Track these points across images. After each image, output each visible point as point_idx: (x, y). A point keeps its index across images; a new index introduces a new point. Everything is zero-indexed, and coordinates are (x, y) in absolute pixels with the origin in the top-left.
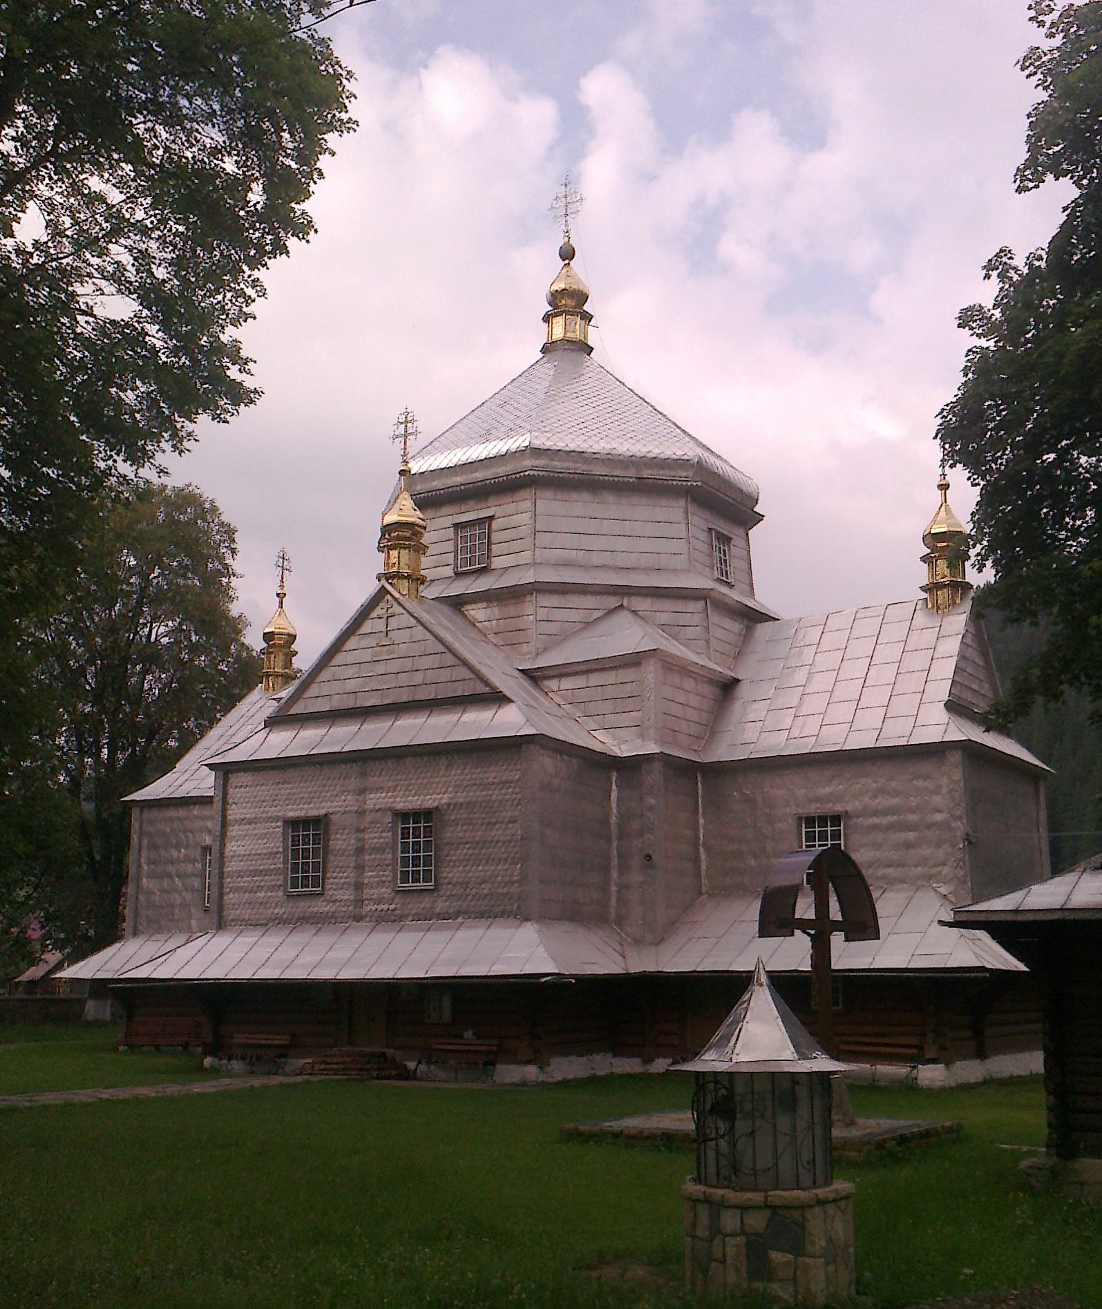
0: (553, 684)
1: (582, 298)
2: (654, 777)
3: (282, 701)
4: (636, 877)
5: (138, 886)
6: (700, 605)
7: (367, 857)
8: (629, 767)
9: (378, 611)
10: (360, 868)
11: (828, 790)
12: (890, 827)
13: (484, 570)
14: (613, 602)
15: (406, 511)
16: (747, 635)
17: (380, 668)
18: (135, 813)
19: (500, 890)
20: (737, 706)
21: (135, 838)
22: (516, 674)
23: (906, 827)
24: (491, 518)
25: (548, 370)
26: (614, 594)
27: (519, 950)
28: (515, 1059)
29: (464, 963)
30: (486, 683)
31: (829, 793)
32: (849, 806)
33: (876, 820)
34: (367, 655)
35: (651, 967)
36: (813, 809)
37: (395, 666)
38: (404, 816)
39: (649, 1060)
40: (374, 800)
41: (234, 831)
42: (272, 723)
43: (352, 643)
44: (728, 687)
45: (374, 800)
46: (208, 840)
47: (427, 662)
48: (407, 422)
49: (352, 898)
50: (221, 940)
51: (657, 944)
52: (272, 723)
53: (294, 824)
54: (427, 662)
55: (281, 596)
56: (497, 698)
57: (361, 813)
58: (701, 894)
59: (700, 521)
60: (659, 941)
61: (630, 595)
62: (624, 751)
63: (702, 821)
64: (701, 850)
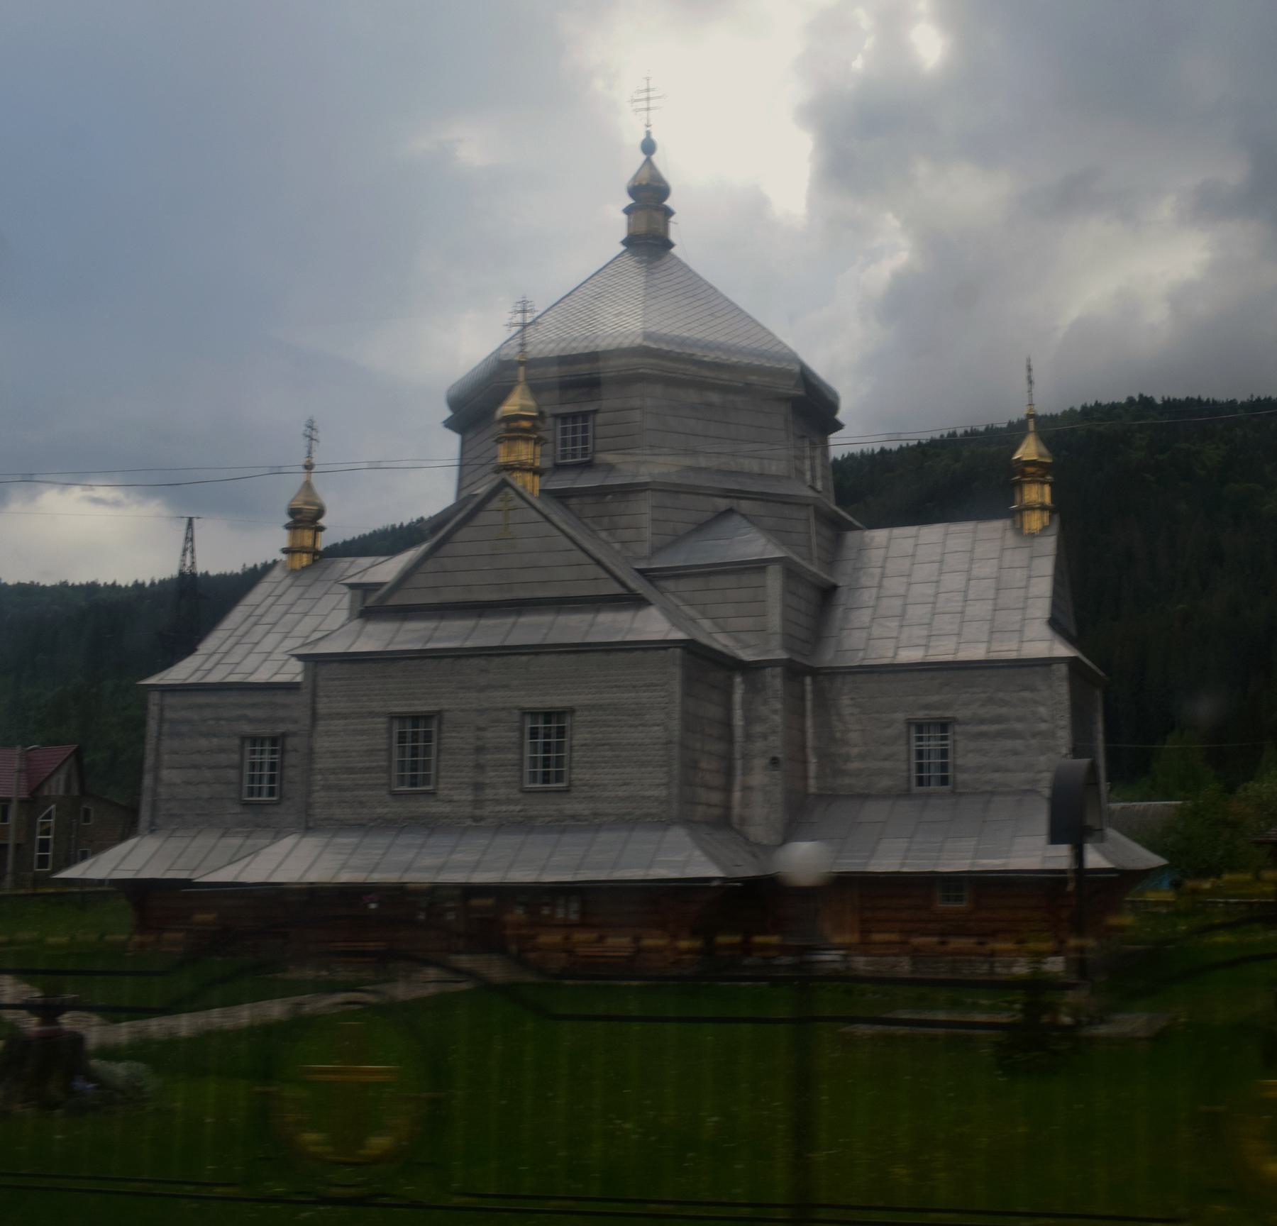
0: (670, 585)
5: (157, 779)
13: (588, 466)
14: (723, 503)
18: (154, 697)
21: (152, 726)
24: (595, 412)
30: (623, 584)
32: (961, 713)
33: (984, 728)
49: (470, 798)
62: (747, 655)
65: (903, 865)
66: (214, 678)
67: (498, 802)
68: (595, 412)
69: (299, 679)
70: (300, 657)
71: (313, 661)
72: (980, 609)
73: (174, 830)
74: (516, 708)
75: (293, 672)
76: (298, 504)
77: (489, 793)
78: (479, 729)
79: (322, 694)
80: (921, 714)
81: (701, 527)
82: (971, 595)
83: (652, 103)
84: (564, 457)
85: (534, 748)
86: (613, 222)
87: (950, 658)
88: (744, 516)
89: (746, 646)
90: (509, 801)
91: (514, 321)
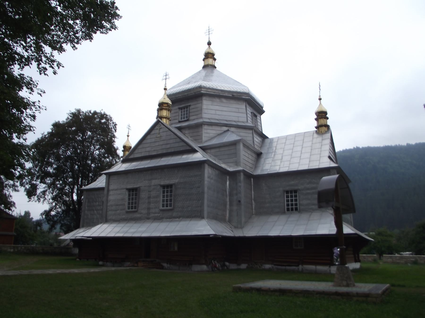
4: (235, 208)
6: (251, 132)
7: (151, 200)
8: (233, 175)
9: (157, 127)
10: (149, 203)
13: (188, 120)
14: (225, 128)
17: (157, 144)
24: (190, 106)
25: (204, 73)
26: (226, 126)
27: (203, 228)
28: (199, 263)
30: (190, 146)
31: (292, 184)
33: (308, 191)
34: (153, 140)
36: (287, 188)
37: (161, 143)
38: (164, 187)
39: (239, 264)
40: (154, 182)
41: (111, 193)
43: (149, 137)
44: (259, 155)
47: (171, 141)
50: (105, 226)
53: (130, 190)
54: (171, 141)
55: (128, 136)
56: (194, 151)
57: (150, 186)
58: (253, 214)
59: (250, 110)
60: (242, 228)
61: (231, 127)
63: (253, 192)
65: (280, 233)
68: (190, 106)
81: (219, 135)
82: (303, 152)
88: (232, 132)
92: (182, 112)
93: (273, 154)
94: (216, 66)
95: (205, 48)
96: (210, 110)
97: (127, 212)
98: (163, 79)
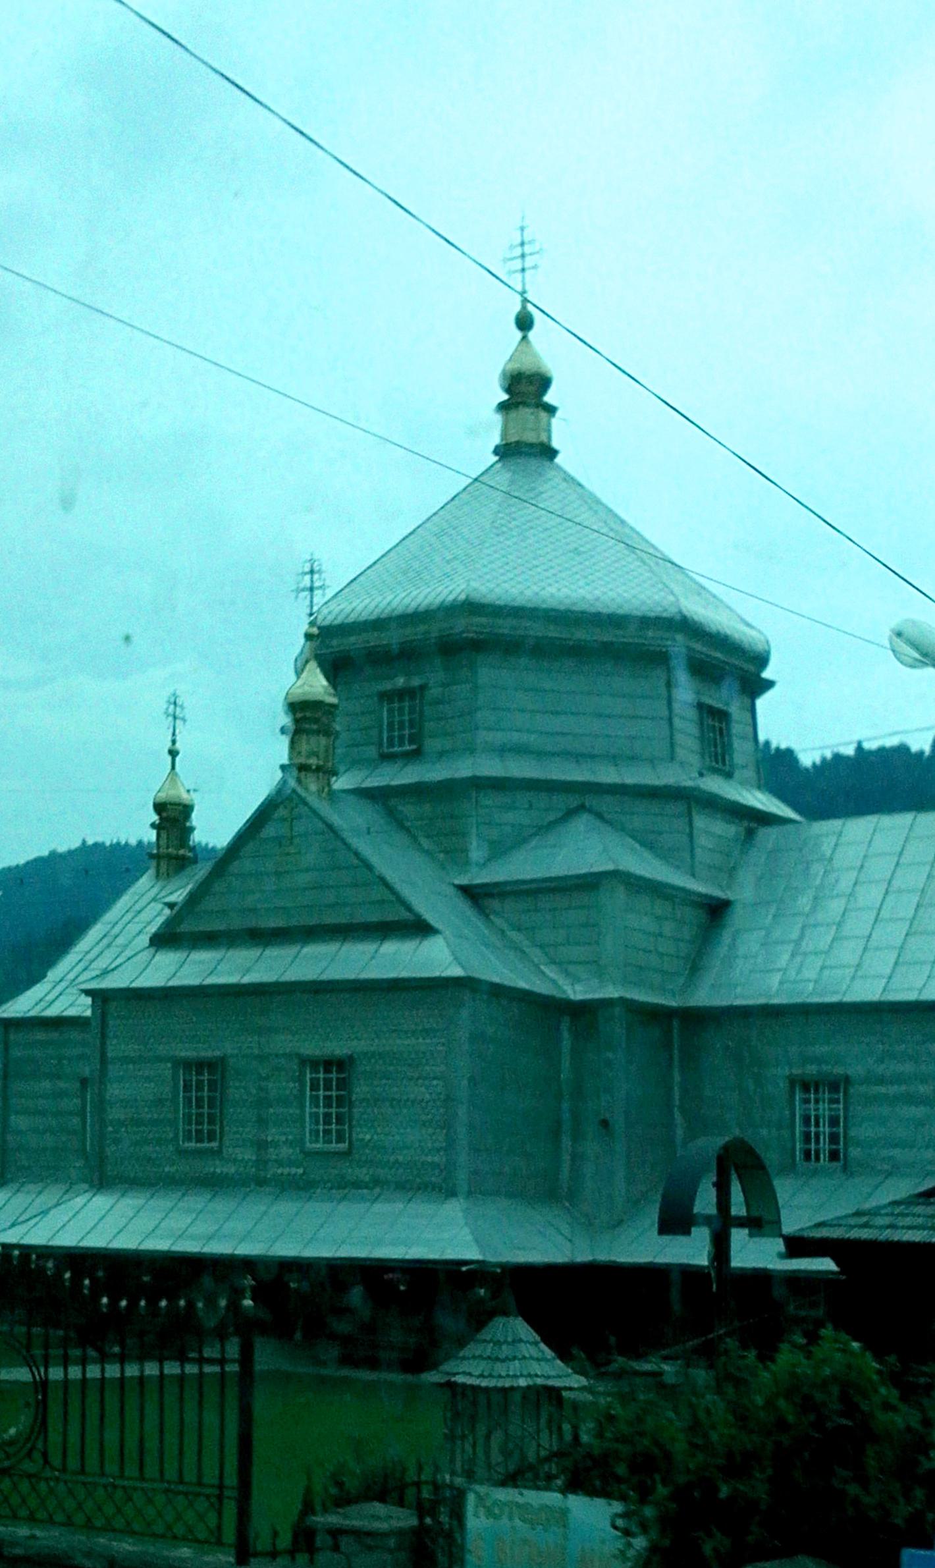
0: (495, 904)
1: (543, 382)
2: (616, 1028)
3: (176, 908)
4: (591, 1147)
11: (826, 1049)
12: (894, 1100)
13: (416, 755)
14: (573, 801)
15: (317, 684)
16: (750, 833)
19: (429, 1159)
20: (726, 936)
22: (451, 891)
23: (911, 1099)
25: (502, 478)
29: (380, 1242)
30: (409, 908)
32: (856, 1070)
35: (602, 1256)
40: (282, 1043)
42: (164, 940)
44: (716, 911)
45: (282, 1043)
46: (87, 1072)
48: (311, 589)
49: (254, 1158)
51: (614, 1227)
52: (164, 940)
55: (173, 753)
56: (420, 928)
62: (577, 993)
63: (677, 1077)
64: (677, 1114)
66: (52, 1012)
67: (280, 1163)
69: (88, 1013)
70: (88, 992)
71: (100, 997)
72: (894, 933)
73: (23, 1184)
74: (288, 1056)
75: (83, 1007)
76: (163, 797)
77: (272, 1153)
78: (261, 1078)
79: (111, 1034)
80: (812, 1069)
82: (885, 914)
83: (529, 261)
84: (401, 744)
85: (315, 1100)
86: (475, 426)
87: (912, 996)
89: (576, 979)
90: (291, 1163)
91: (302, 586)
92: (390, 711)
93: (773, 910)
94: (555, 444)
95: (500, 349)
96: (507, 728)
97: (183, 1153)
98: (300, 590)
